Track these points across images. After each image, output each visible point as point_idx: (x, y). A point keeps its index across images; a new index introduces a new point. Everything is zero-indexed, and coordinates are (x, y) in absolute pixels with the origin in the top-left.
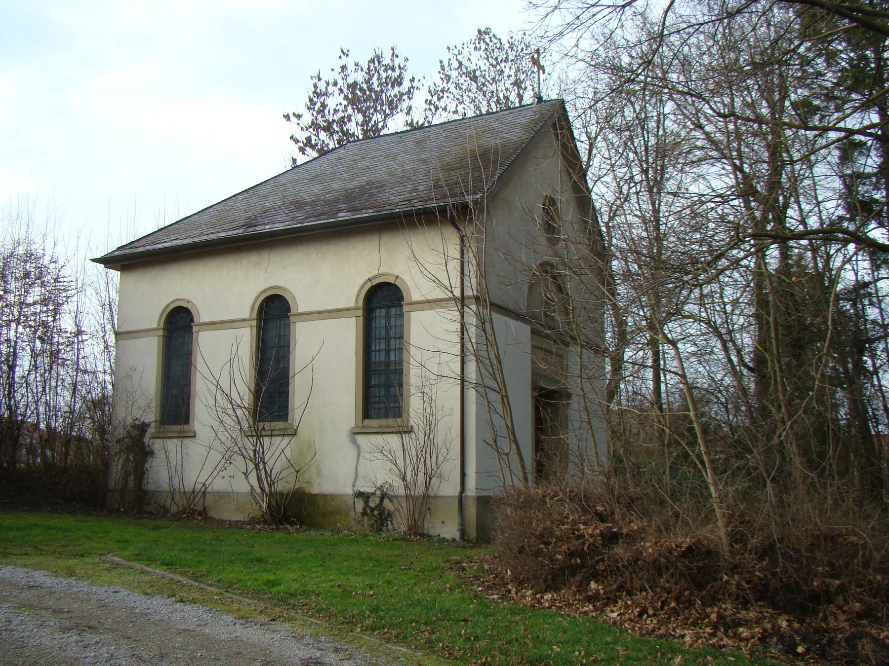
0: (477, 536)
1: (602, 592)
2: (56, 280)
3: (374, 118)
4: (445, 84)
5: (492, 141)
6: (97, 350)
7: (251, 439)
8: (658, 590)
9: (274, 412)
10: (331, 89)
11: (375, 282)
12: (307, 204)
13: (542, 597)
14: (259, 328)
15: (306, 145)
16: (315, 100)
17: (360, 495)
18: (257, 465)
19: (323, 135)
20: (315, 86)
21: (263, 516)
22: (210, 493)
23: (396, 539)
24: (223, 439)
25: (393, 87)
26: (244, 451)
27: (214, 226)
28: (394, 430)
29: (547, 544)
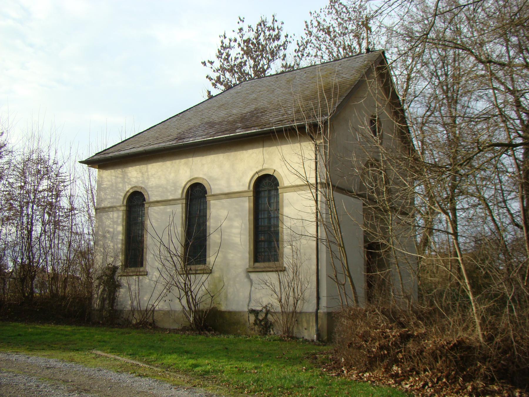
1: (400, 372)
2: (57, 175)
3: (261, 63)
4: (309, 38)
5: (335, 80)
6: (83, 219)
7: (182, 276)
8: (435, 371)
9: (197, 259)
10: (232, 44)
11: (261, 174)
12: (215, 124)
13: (363, 375)
14: (187, 204)
15: (216, 82)
16: (222, 51)
17: (252, 311)
18: (186, 293)
19: (228, 75)
20: (222, 42)
21: (191, 326)
22: (157, 311)
23: (275, 340)
24: (165, 276)
25: (274, 41)
26: (178, 284)
27: (157, 139)
28: (274, 269)
29: (366, 341)
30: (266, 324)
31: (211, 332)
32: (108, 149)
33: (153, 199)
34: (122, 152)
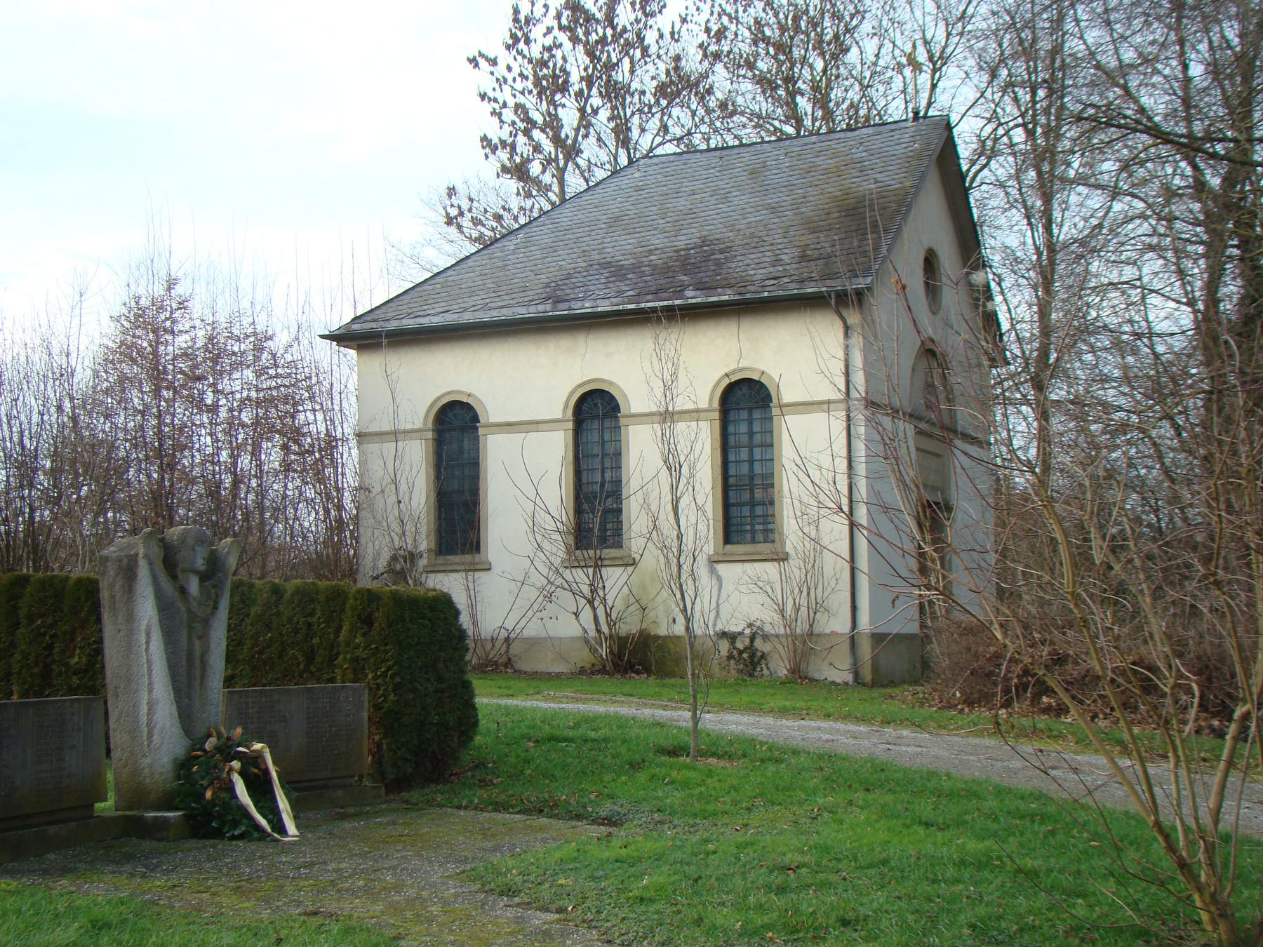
0: (873, 680)
17: (724, 635)
28: (770, 556)
30: (752, 656)
32: (377, 308)
33: (495, 418)
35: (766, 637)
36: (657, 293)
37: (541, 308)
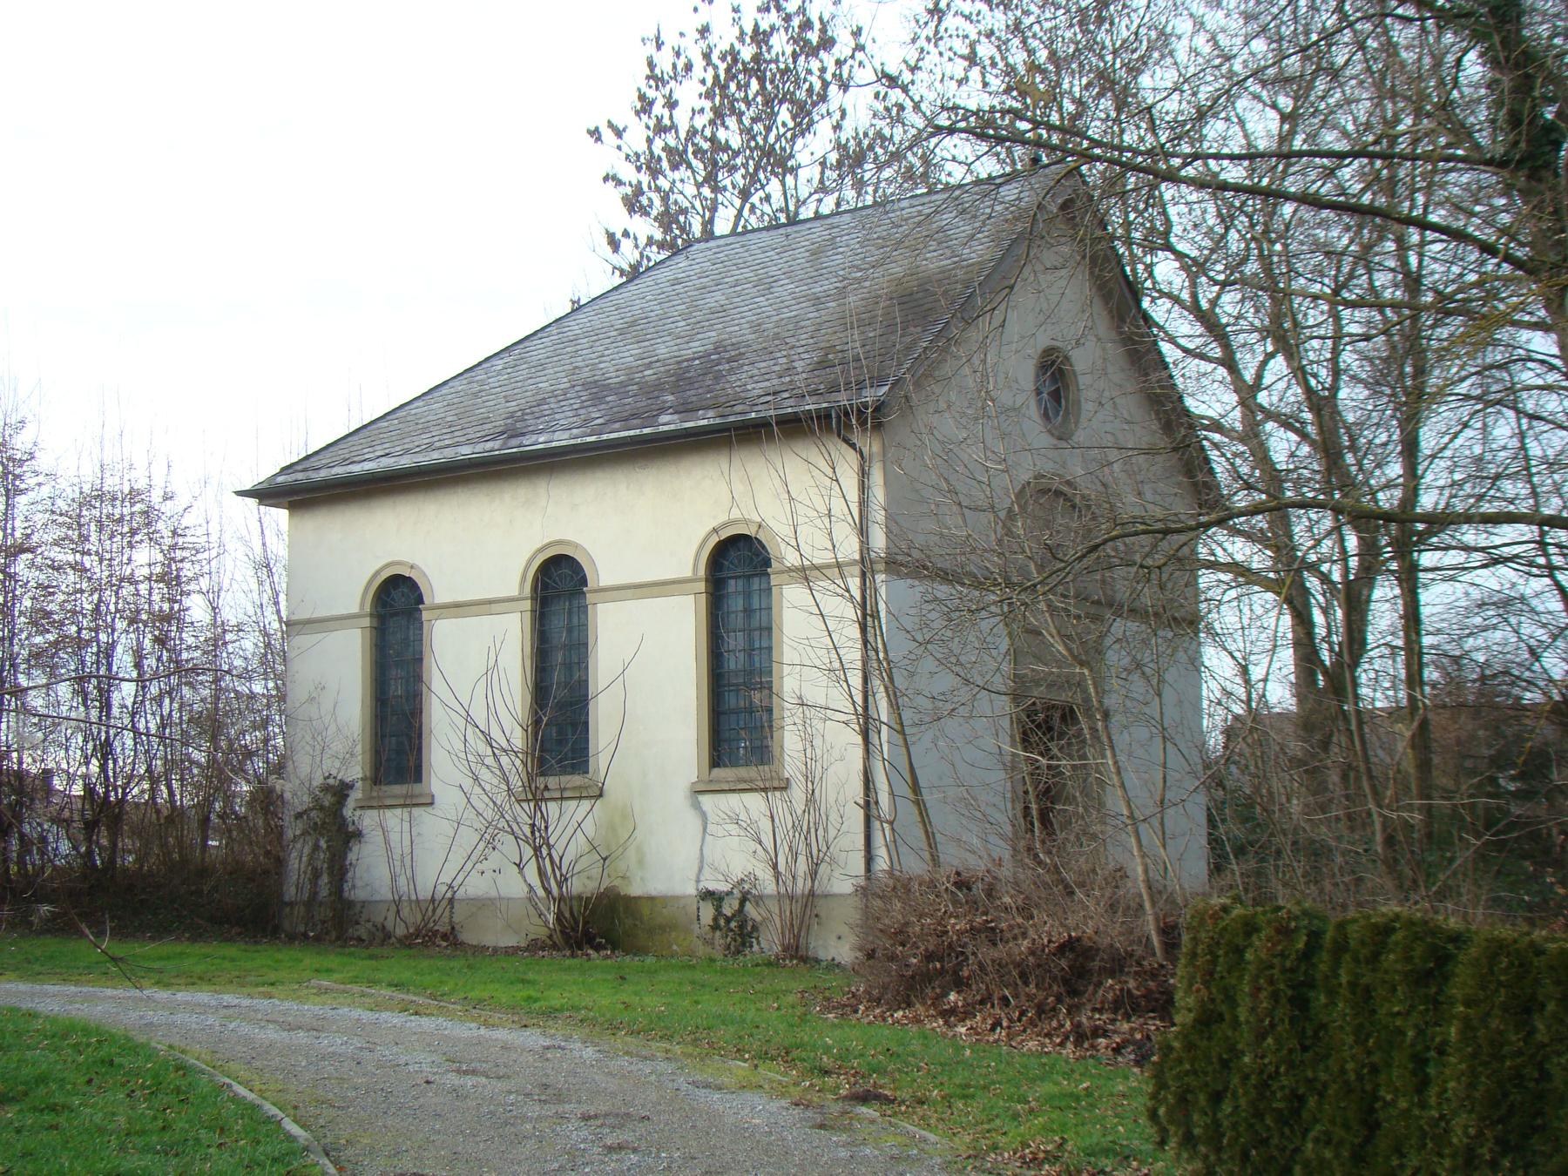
7: (525, 805)
11: (725, 534)
17: (708, 895)
18: (537, 850)
20: (651, 65)
21: (550, 937)
23: (757, 965)
24: (480, 806)
30: (741, 926)
31: (603, 953)
32: (316, 453)
34: (356, 469)
35: (759, 899)
36: (626, 420)
37: (489, 445)
